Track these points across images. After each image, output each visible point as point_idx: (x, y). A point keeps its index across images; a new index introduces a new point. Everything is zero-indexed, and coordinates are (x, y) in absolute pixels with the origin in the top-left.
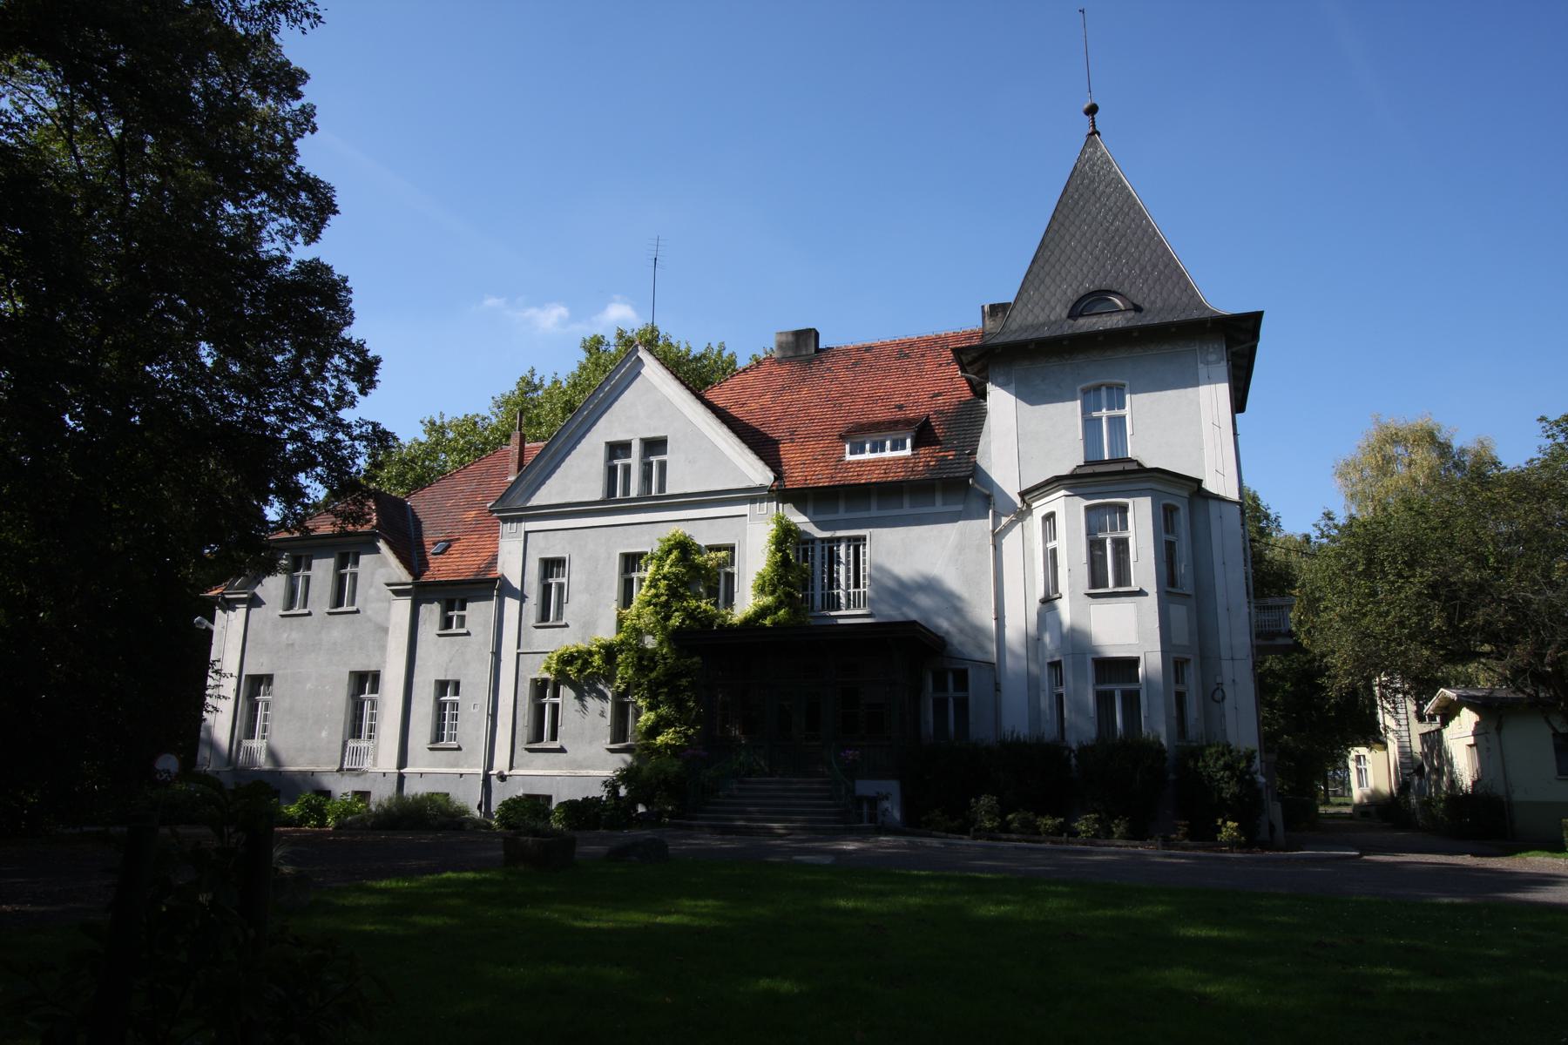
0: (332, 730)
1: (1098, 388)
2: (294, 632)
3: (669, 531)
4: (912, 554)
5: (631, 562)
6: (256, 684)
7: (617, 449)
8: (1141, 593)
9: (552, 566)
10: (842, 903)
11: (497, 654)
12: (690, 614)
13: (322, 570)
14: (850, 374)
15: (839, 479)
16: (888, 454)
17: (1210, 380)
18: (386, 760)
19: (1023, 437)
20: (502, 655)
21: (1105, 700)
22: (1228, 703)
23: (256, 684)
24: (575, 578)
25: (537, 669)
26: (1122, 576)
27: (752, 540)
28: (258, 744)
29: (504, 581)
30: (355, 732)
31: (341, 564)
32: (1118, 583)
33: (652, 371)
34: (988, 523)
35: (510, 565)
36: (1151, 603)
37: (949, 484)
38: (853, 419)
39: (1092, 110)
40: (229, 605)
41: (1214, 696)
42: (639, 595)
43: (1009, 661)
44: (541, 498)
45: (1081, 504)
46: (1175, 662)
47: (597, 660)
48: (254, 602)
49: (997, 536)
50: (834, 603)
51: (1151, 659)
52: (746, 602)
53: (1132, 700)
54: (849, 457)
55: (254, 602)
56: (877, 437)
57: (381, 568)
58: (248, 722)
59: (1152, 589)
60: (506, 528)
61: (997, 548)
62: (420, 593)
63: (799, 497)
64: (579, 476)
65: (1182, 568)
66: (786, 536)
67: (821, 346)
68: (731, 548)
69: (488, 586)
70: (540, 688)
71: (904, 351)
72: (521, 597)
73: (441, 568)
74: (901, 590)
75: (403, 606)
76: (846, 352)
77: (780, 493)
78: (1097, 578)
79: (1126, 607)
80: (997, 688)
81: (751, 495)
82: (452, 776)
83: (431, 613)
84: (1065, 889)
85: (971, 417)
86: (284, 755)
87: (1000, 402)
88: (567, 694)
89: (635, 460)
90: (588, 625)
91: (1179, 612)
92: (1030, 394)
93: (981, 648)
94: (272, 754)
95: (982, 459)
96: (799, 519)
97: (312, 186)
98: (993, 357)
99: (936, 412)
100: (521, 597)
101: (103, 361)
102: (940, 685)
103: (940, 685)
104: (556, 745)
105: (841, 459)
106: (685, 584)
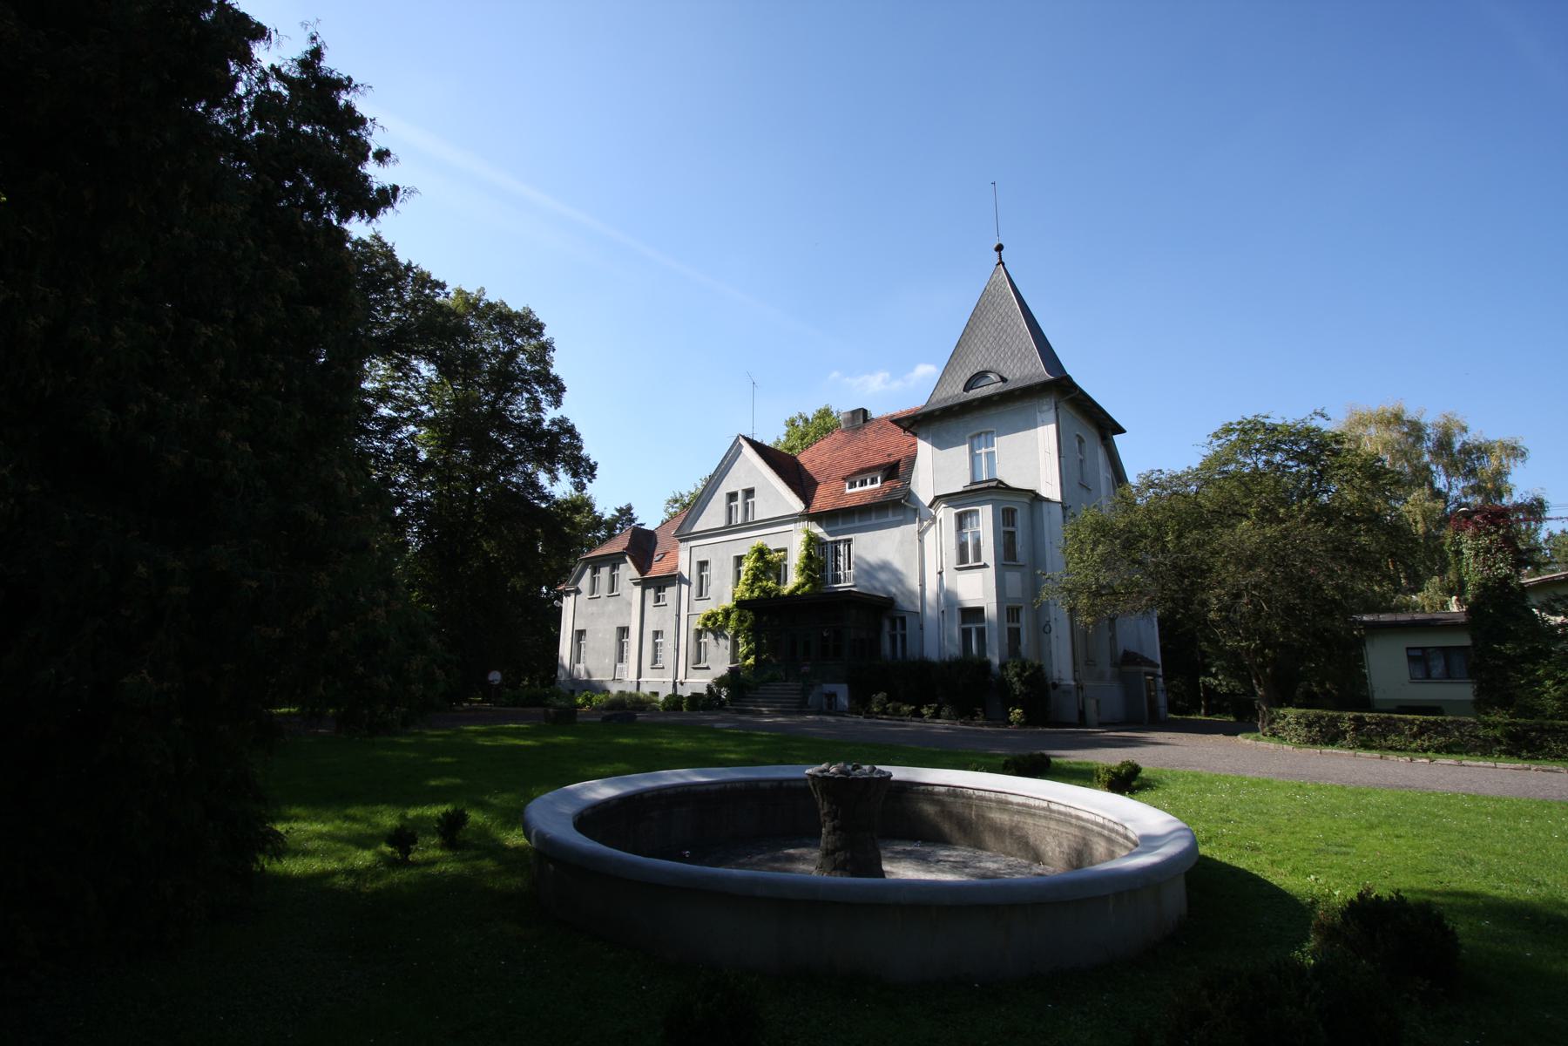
0: (609, 660)
2: (593, 608)
3: (757, 542)
4: (877, 549)
5: (739, 560)
6: (580, 634)
7: (732, 496)
8: (985, 566)
9: (703, 565)
11: (678, 616)
12: (763, 590)
13: (605, 572)
16: (869, 487)
17: (1044, 423)
18: (633, 677)
19: (937, 469)
20: (680, 614)
21: (966, 634)
22: (1053, 634)
23: (580, 634)
24: (712, 571)
25: (697, 624)
26: (978, 557)
27: (793, 543)
28: (581, 667)
29: (681, 575)
30: (621, 660)
31: (613, 569)
33: (747, 450)
34: (915, 527)
35: (684, 569)
37: (896, 506)
39: (999, 248)
40: (568, 594)
41: (1042, 629)
42: (743, 578)
43: (928, 611)
44: (697, 527)
45: (954, 511)
46: (1009, 611)
47: (720, 618)
48: (578, 592)
49: (921, 533)
50: (837, 579)
51: (991, 610)
52: (793, 580)
53: (981, 633)
54: (848, 491)
55: (578, 592)
56: (863, 477)
57: (628, 571)
58: (577, 656)
59: (991, 564)
60: (682, 545)
61: (921, 541)
62: (645, 584)
63: (818, 518)
64: (713, 515)
65: (1020, 548)
66: (812, 541)
68: (785, 550)
69: (673, 579)
70: (699, 633)
72: (689, 584)
73: (658, 569)
74: (870, 571)
75: (638, 589)
77: (808, 516)
78: (963, 557)
79: (977, 574)
80: (922, 628)
82: (657, 683)
83: (650, 593)
86: (593, 672)
87: (924, 449)
88: (710, 636)
89: (739, 502)
90: (720, 598)
91: (1014, 578)
92: (940, 444)
93: (913, 603)
94: (588, 673)
95: (913, 487)
96: (818, 530)
97: (556, 380)
100: (689, 584)
101: (427, 502)
102: (894, 627)
103: (894, 627)
106: (763, 573)
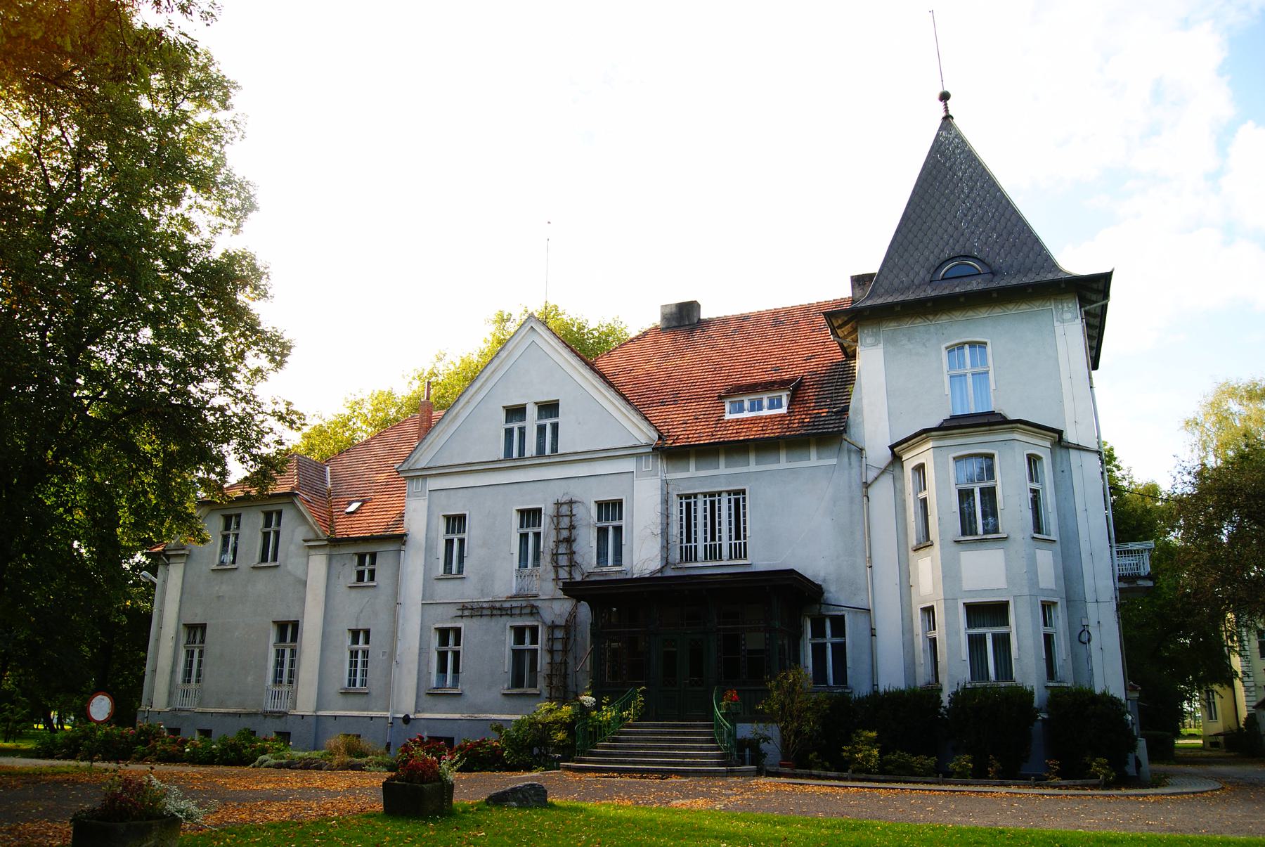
1: (961, 346)
102: (818, 631)
103: (818, 631)
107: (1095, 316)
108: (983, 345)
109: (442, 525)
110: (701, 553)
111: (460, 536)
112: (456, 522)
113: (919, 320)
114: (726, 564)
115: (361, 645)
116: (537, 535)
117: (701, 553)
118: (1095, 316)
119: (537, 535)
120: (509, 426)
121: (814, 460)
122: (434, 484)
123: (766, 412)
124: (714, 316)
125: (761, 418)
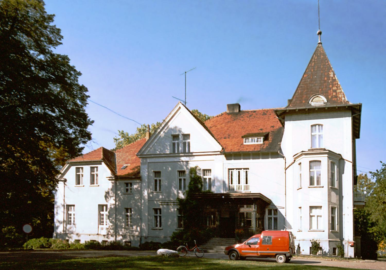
1: (315, 125)
10: (143, 150)
14: (248, 119)
15: (241, 150)
26: (318, 183)
32: (318, 184)
36: (325, 190)
38: (247, 132)
67: (241, 110)
71: (265, 113)
76: (248, 112)
81: (214, 153)
84: (218, 195)
85: (279, 134)
98: (283, 115)
99: (272, 131)
102: (270, 213)
103: (270, 213)
104: (160, 228)
105: (242, 144)
107: (357, 119)
108: (322, 125)
109: (152, 175)
110: (243, 188)
111: (160, 178)
112: (157, 173)
113: (304, 115)
114: (243, 191)
115: (158, 214)
116: (184, 180)
117: (243, 188)
118: (357, 119)
119: (184, 180)
120: (174, 142)
121: (270, 161)
122: (148, 160)
123: (256, 143)
124: (244, 110)
125: (254, 145)
